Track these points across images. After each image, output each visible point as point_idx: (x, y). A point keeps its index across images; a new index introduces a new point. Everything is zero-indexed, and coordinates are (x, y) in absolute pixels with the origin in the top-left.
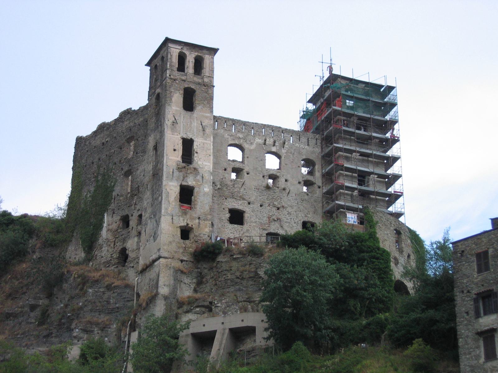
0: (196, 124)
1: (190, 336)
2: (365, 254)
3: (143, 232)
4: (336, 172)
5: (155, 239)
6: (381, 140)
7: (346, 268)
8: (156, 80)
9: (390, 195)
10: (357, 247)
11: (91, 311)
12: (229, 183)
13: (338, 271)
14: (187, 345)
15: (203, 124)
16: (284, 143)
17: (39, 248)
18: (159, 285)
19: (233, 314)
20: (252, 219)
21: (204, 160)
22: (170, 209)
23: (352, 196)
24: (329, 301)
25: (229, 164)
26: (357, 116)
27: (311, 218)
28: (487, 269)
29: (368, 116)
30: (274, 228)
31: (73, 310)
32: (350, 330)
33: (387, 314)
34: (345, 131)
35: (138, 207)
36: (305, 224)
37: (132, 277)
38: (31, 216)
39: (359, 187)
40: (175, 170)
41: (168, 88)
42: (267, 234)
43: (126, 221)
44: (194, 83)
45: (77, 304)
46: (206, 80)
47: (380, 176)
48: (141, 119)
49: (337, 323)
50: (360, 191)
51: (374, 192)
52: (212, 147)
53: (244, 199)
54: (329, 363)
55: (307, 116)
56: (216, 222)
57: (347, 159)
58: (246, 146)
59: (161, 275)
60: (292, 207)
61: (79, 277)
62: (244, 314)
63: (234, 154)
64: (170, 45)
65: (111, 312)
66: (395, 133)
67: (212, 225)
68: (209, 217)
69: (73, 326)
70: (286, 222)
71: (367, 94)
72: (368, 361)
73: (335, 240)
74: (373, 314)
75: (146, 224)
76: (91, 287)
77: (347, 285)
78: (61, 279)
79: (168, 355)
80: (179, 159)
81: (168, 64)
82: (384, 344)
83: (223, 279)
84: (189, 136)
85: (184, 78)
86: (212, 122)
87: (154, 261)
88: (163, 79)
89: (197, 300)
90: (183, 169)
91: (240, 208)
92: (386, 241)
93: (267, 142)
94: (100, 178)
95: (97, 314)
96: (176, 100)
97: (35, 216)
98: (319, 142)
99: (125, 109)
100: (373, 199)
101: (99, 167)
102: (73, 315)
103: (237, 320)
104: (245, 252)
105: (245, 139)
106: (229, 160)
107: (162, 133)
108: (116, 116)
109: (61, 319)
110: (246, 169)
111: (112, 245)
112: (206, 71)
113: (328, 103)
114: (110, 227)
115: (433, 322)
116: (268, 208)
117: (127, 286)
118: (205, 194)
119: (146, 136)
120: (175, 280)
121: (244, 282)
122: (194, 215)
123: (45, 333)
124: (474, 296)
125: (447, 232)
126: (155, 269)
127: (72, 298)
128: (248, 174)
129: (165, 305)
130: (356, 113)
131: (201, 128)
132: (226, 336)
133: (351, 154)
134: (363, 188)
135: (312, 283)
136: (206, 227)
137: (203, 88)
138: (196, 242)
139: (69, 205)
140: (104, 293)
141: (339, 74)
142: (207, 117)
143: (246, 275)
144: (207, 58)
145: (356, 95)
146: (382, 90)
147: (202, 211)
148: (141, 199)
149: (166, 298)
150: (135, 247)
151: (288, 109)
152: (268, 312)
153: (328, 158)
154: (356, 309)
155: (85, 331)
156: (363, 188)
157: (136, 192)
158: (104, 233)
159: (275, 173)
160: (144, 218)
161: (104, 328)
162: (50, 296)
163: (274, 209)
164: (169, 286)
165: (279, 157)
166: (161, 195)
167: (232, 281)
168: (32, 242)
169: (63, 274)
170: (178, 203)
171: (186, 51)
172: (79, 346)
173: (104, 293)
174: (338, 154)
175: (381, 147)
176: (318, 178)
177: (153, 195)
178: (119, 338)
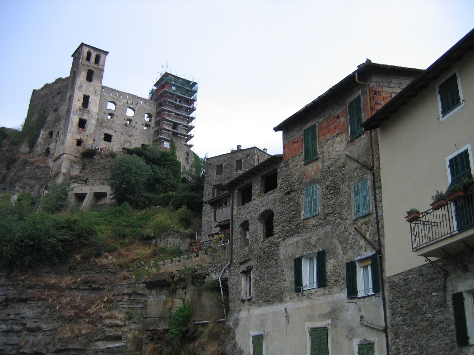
0: (92, 89)
1: (74, 195)
2: (168, 162)
3: (58, 141)
4: (162, 121)
5: (63, 144)
6: (187, 109)
7: (156, 168)
8: (75, 64)
9: (188, 136)
10: (164, 158)
11: (27, 178)
12: (106, 120)
13: (152, 169)
14: (72, 200)
15: (96, 89)
16: (137, 104)
17: (8, 145)
18: (62, 167)
19: (97, 185)
20: (116, 140)
21: (94, 107)
22: (72, 130)
23: (168, 134)
24: (145, 184)
25: (107, 111)
26: (176, 95)
27: (146, 143)
28: (221, 173)
29: (182, 95)
30: (127, 146)
31: (18, 177)
32: (154, 199)
33: (174, 193)
34: (169, 101)
35: (58, 128)
36: (143, 145)
37: (51, 163)
38: (7, 128)
39: (173, 130)
40: (78, 110)
41: (79, 68)
42: (123, 148)
43: (51, 134)
44: (94, 67)
45: (21, 174)
46: (100, 67)
47: (184, 126)
48: (66, 83)
49: (149, 195)
50: (173, 132)
51: (180, 133)
52: (99, 101)
53: (113, 129)
54: (139, 214)
55: (153, 93)
56: (96, 139)
57: (169, 115)
58: (117, 103)
59: (63, 163)
60: (137, 136)
61: (23, 160)
62: (103, 186)
63: (111, 106)
64: (84, 47)
65: (37, 179)
66: (194, 105)
67: (94, 140)
68: (93, 136)
69: (16, 185)
70: (133, 143)
71: (183, 85)
72: (159, 214)
73: (153, 153)
74: (167, 192)
75: (60, 136)
76: (29, 166)
77: (156, 177)
78: (14, 161)
79: (59, 203)
80: (81, 105)
81: (81, 56)
82: (170, 207)
83: (95, 168)
84: (88, 94)
85: (88, 64)
86: (100, 88)
87: (61, 155)
88: (78, 64)
89: (80, 177)
90: (82, 110)
91: (110, 133)
92: (180, 157)
93: (129, 102)
94: (42, 111)
95: (30, 180)
96: (83, 75)
97: (9, 128)
98: (156, 105)
99: (58, 77)
100: (179, 137)
101: (42, 106)
102: (17, 179)
103: (99, 188)
104: (108, 155)
105: (117, 99)
106: (108, 109)
107: (73, 91)
108: (54, 81)
109: (12, 181)
110: (116, 114)
111: (43, 146)
112: (101, 63)
113: (163, 87)
114: (43, 137)
115: (194, 198)
116: (125, 135)
117: (47, 167)
118: (92, 124)
119: (66, 92)
120: (70, 166)
121: (105, 170)
122: (85, 134)
123: (3, 187)
124: (213, 186)
125: (207, 154)
126: (61, 160)
127: (18, 170)
128: (116, 117)
129: (63, 178)
130: (176, 93)
131: (94, 91)
132: (91, 196)
133: (171, 113)
134: (175, 131)
135: (136, 173)
136: (90, 141)
137: (99, 71)
138: (84, 148)
139: (25, 124)
140: (35, 169)
141: (170, 73)
142: (98, 86)
143: (107, 167)
144: (102, 56)
145: (177, 84)
146: (191, 84)
147: (89, 132)
148: (60, 124)
149: (64, 174)
150: (54, 148)
151: (144, 89)
152: (112, 186)
153: (159, 114)
154: (159, 189)
155: (22, 188)
156: (175, 131)
157: (57, 120)
158: (40, 140)
159: (130, 118)
160: (60, 133)
161: (32, 187)
162: (8, 169)
163: (128, 136)
164: (66, 168)
165: (134, 110)
166: (69, 122)
167: (99, 169)
168: (5, 141)
169: (16, 158)
170: (77, 127)
171: (92, 51)
172: (17, 195)
173: (35, 169)
174: (164, 113)
175: (186, 112)
176: (153, 124)
177: (65, 122)
178: (39, 192)
